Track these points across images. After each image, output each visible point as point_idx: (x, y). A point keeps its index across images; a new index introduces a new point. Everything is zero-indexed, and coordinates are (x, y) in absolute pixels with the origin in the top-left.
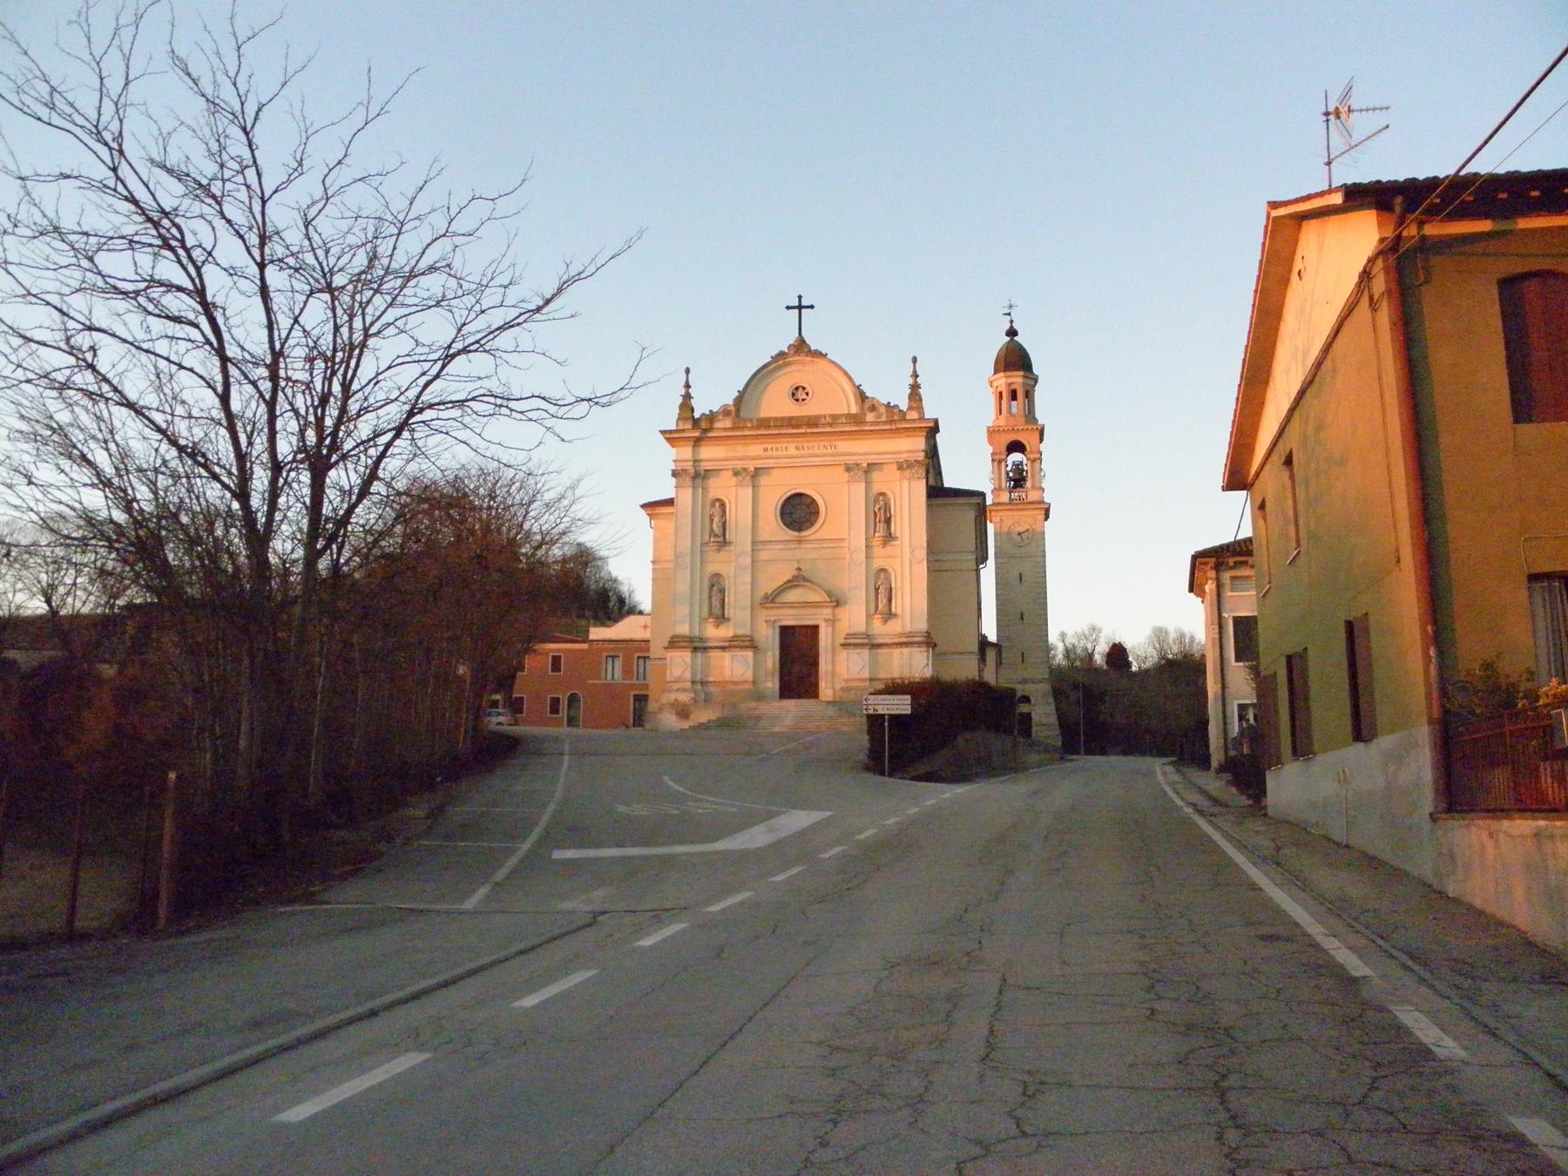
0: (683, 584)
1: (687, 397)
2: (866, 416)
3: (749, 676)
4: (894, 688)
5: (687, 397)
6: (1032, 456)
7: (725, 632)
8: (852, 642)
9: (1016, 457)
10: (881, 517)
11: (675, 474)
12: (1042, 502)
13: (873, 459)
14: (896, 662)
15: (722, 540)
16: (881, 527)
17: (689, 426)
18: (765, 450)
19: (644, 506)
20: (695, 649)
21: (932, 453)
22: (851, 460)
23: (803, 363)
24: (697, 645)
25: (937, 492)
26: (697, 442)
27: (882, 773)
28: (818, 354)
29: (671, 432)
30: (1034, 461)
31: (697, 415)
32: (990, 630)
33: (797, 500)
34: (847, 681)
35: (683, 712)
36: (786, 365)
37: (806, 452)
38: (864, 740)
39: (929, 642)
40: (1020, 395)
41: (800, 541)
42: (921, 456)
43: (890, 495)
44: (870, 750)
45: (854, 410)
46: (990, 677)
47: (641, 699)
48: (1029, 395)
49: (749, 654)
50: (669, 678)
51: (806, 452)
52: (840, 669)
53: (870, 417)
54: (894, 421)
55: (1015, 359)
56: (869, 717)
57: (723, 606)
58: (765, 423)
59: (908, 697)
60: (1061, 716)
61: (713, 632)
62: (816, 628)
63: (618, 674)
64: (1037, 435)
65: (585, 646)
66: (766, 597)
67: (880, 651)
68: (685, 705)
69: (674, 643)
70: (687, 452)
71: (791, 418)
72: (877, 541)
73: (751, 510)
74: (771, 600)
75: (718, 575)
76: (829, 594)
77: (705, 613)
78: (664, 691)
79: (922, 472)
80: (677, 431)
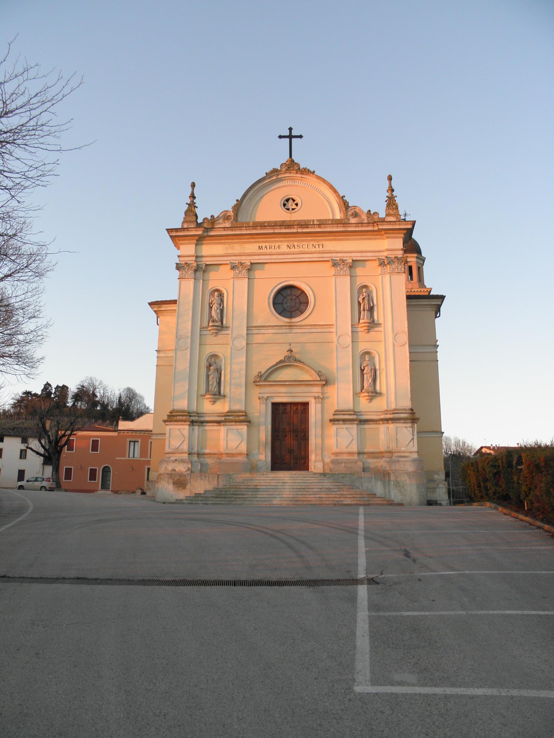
0: (183, 364)
1: (192, 206)
2: (351, 222)
3: (243, 448)
5: (192, 206)
7: (222, 407)
8: (340, 419)
10: (365, 306)
11: (179, 267)
13: (357, 256)
14: (382, 436)
15: (220, 326)
16: (365, 315)
20: (193, 423)
23: (293, 179)
24: (195, 420)
26: (200, 240)
28: (306, 171)
29: (177, 230)
31: (200, 220)
33: (289, 291)
34: (336, 454)
35: (180, 482)
37: (297, 250)
41: (291, 326)
43: (373, 288)
49: (244, 428)
50: (167, 450)
52: (328, 443)
53: (353, 220)
54: (373, 226)
57: (219, 384)
61: (210, 408)
62: (306, 405)
63: (137, 454)
65: (115, 434)
66: (260, 376)
67: (366, 426)
68: (181, 475)
69: (173, 417)
72: (361, 328)
73: (247, 299)
74: (264, 379)
75: (215, 356)
76: (319, 374)
77: (203, 391)
78: (162, 461)
80: (182, 229)
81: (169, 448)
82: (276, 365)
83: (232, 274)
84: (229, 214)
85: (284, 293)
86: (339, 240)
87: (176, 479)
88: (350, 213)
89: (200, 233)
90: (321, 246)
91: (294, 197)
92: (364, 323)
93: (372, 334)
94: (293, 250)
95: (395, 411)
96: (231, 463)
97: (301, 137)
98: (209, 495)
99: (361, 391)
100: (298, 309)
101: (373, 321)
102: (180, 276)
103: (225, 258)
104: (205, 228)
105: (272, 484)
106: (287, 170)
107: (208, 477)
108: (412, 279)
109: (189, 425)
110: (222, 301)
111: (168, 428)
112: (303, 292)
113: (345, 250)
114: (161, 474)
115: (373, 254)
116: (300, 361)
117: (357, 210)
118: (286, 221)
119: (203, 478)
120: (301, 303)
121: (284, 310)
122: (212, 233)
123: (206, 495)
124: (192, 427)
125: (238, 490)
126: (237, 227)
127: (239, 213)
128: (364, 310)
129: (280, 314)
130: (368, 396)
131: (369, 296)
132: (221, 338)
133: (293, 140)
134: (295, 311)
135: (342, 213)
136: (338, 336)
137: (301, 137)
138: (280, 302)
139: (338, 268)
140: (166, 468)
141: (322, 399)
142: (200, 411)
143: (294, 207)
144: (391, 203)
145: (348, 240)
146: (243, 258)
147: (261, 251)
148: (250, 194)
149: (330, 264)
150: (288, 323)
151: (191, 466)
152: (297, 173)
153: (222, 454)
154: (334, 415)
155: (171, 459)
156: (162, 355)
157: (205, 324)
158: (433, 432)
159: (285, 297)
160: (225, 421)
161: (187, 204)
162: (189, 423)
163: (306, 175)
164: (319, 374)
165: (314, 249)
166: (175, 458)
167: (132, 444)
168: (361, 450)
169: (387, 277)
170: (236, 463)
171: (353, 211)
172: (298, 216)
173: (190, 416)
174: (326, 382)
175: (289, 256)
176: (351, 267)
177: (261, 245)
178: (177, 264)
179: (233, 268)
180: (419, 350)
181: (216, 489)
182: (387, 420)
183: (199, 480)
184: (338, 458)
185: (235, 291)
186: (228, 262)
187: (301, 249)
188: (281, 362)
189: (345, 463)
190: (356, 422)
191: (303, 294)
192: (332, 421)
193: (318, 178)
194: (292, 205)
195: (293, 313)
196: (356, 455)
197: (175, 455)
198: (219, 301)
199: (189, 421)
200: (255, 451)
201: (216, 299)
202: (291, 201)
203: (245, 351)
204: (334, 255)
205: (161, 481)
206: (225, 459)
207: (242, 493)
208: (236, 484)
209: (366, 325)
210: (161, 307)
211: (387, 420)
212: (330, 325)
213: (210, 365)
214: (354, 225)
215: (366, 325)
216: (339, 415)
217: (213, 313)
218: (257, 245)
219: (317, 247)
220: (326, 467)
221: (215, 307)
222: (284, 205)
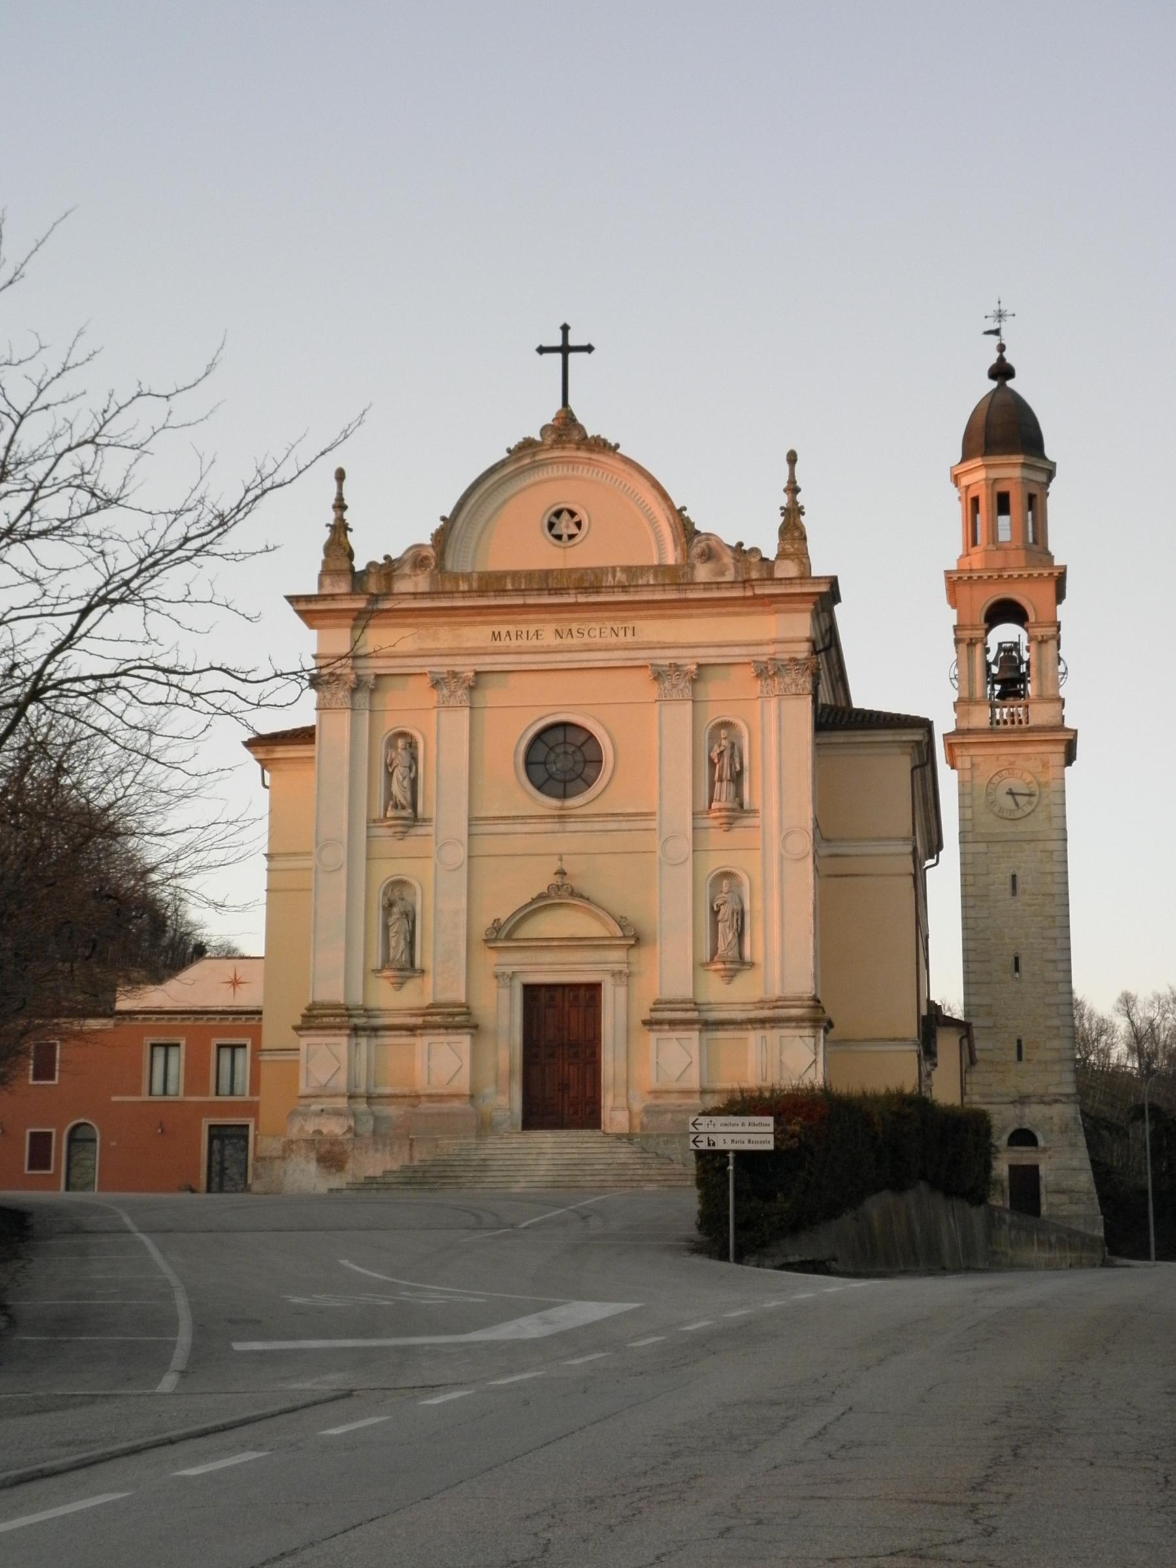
1: (340, 529)
2: (699, 573)
4: (744, 1104)
5: (340, 529)
6: (1039, 632)
9: (1007, 633)
10: (725, 767)
12: (1060, 727)
15: (408, 814)
16: (724, 790)
17: (343, 587)
18: (496, 636)
19: (249, 744)
20: (356, 1030)
21: (827, 644)
22: (664, 658)
24: (357, 1023)
25: (837, 719)
26: (361, 619)
27: (723, 1256)
28: (600, 446)
29: (308, 598)
30: (1042, 642)
31: (359, 565)
32: (947, 988)
33: (559, 735)
34: (656, 1093)
35: (331, 1158)
36: (536, 466)
37: (575, 641)
38: (691, 1201)
39: (818, 1017)
40: (1017, 502)
42: (802, 651)
44: (701, 1214)
45: (671, 557)
46: (945, 1091)
47: (229, 1139)
48: (1035, 502)
50: (303, 1089)
51: (575, 641)
52: (644, 1070)
53: (703, 572)
55: (1006, 430)
56: (700, 1154)
57: (411, 944)
58: (492, 583)
59: (770, 1120)
60: (1101, 1172)
61: (389, 999)
62: (594, 989)
63: (177, 1084)
64: (1050, 589)
66: (497, 927)
67: (720, 1034)
68: (334, 1142)
69: (315, 1019)
70: (340, 640)
71: (547, 573)
73: (469, 755)
74: (502, 935)
77: (376, 961)
78: (293, 1114)
79: (806, 682)
81: (307, 1086)
82: (530, 904)
83: (435, 698)
84: (424, 554)
85: (551, 738)
86: (670, 617)
87: (323, 1150)
88: (696, 551)
89: (361, 604)
90: (629, 632)
91: (574, 508)
92: (720, 810)
93: (737, 833)
94: (568, 641)
95: (779, 1002)
96: (439, 1114)
97: (589, 349)
98: (392, 1180)
99: (712, 959)
100: (579, 776)
101: (741, 805)
102: (319, 703)
103: (418, 661)
104: (372, 594)
105: (516, 1157)
106: (555, 442)
107: (391, 1144)
108: (975, 543)
109: (349, 1036)
110: (414, 758)
111: (303, 1043)
112: (591, 736)
113: (682, 640)
114: (292, 1142)
116: (582, 896)
117: (713, 543)
118: (552, 571)
119: (380, 1147)
120: (585, 762)
121: (551, 777)
122: (387, 605)
123: (387, 1180)
124: (354, 1040)
125: (448, 1169)
126: (443, 593)
127: (447, 550)
128: (721, 780)
129: (539, 788)
130: (725, 970)
131: (733, 745)
132: (411, 844)
134: (573, 780)
135: (679, 548)
136: (663, 839)
137: (589, 349)
138: (542, 759)
139: (667, 684)
140: (302, 1129)
141: (629, 975)
142: (372, 1004)
143: (573, 530)
145: (690, 616)
146: (459, 660)
147: (498, 643)
148: (472, 501)
149: (648, 673)
150: (556, 808)
151: (355, 1122)
152: (578, 449)
153: (418, 1096)
154: (652, 1010)
155: (313, 1108)
156: (281, 864)
157: (378, 812)
158: (894, 1040)
159: (551, 749)
160: (425, 1027)
161: (328, 525)
162: (348, 1032)
163: (599, 453)
164: (622, 923)
165: (613, 640)
166: (320, 1107)
167: (159, 1053)
168: (707, 1085)
169: (774, 702)
170: (448, 1114)
171: (703, 545)
172: (582, 555)
173: (350, 1016)
174: (638, 940)
175: (559, 657)
176: (694, 681)
177: (496, 628)
179: (436, 684)
180: (875, 850)
181: (405, 1168)
182: (763, 1022)
183: (371, 1153)
184: (660, 1101)
185: (445, 736)
186: (426, 670)
187: (586, 639)
188: (541, 897)
189: (673, 1112)
190: (697, 1027)
191: (561, 793)
192: (649, 1023)
193: (627, 461)
194: (567, 527)
195: (569, 787)
196: (697, 1096)
197: (321, 1100)
199: (347, 1028)
200: (489, 1090)
201: (402, 757)
202: (565, 516)
203: (465, 875)
204: (658, 653)
205: (293, 1156)
206: (425, 1106)
207: (456, 1174)
208: (446, 1157)
209: (724, 814)
210: (273, 752)
211: (763, 1022)
212: (647, 814)
213: (391, 905)
214: (702, 586)
215: (724, 814)
216: (663, 1010)
217: (395, 788)
218: (487, 630)
219: (621, 633)
220: (636, 1122)
221: (398, 774)
222: (551, 526)
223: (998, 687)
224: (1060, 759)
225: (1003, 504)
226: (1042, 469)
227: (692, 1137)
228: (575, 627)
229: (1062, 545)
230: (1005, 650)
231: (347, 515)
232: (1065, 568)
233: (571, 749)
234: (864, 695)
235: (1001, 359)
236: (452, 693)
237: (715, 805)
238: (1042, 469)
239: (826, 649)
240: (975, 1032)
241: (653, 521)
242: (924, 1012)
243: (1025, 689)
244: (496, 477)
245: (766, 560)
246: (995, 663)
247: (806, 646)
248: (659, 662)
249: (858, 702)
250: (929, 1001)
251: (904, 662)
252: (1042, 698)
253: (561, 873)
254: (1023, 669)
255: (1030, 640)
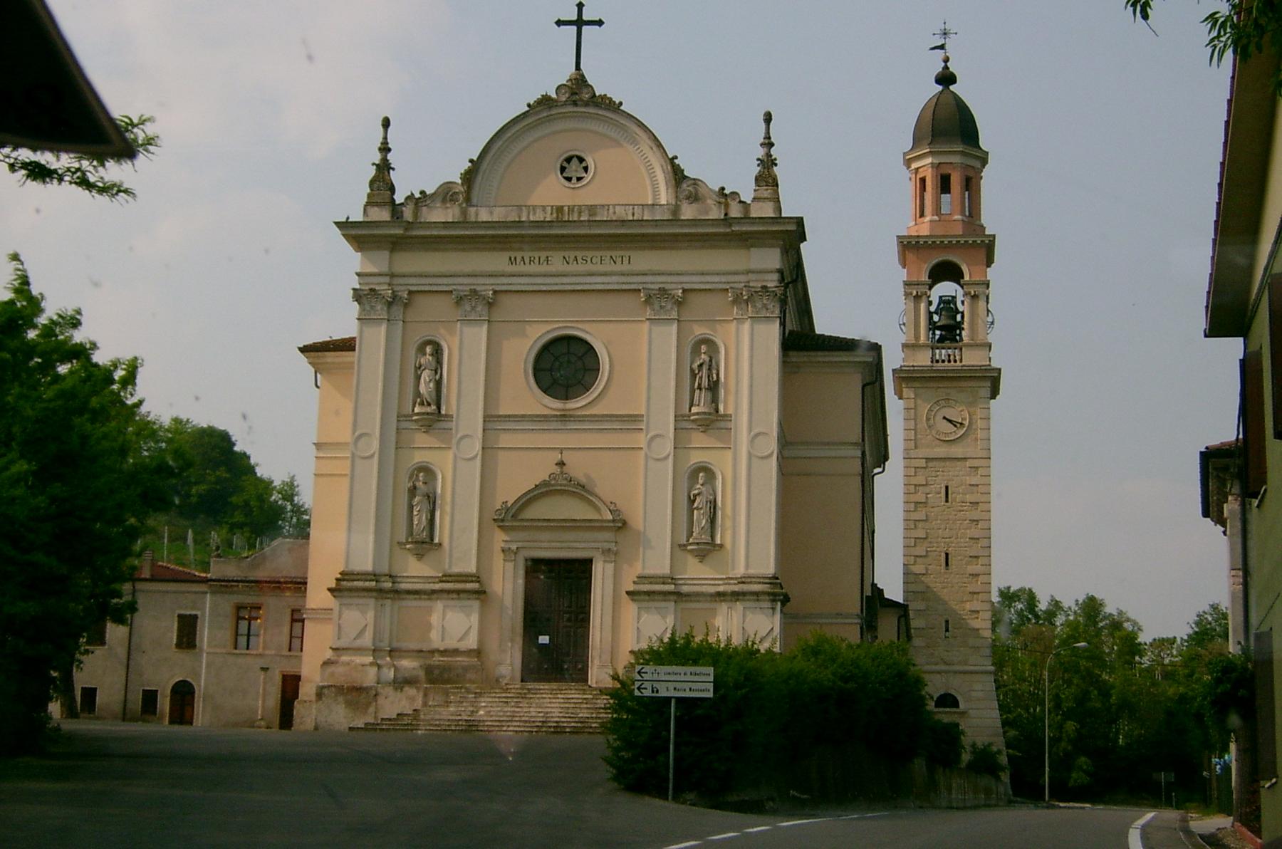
1: (384, 167)
5: (384, 167)
8: (648, 593)
9: (946, 288)
11: (358, 296)
15: (434, 416)
22: (655, 283)
25: (801, 341)
36: (550, 119)
37: (581, 268)
39: (777, 593)
42: (772, 281)
48: (971, 184)
52: (621, 631)
55: (950, 128)
61: (415, 570)
64: (982, 255)
70: (379, 262)
74: (510, 518)
89: (400, 231)
90: (626, 260)
91: (583, 155)
92: (697, 414)
108: (922, 215)
115: (723, 279)
120: (586, 370)
121: (555, 382)
124: (380, 602)
133: (585, 28)
144: (767, 176)
159: (557, 358)
169: (746, 326)
177: (513, 255)
178: (354, 289)
198: (434, 364)
201: (427, 359)
202: (575, 161)
217: (423, 389)
221: (426, 375)
222: (563, 169)
223: (938, 332)
224: (986, 392)
225: (945, 185)
226: (977, 158)
227: (637, 684)
228: (579, 254)
229: (990, 220)
230: (945, 302)
231: (389, 156)
232: (994, 236)
233: (573, 359)
234: (824, 325)
235: (946, 68)
236: (473, 308)
237: (694, 410)
238: (977, 158)
239: (794, 281)
240: (911, 614)
241: (650, 168)
242: (868, 592)
243: (960, 335)
244: (517, 127)
245: (744, 202)
246: (936, 313)
247: (776, 276)
248: (652, 286)
249: (820, 329)
250: (874, 585)
251: (861, 294)
252: (975, 345)
253: (561, 464)
254: (959, 318)
255: (966, 294)
